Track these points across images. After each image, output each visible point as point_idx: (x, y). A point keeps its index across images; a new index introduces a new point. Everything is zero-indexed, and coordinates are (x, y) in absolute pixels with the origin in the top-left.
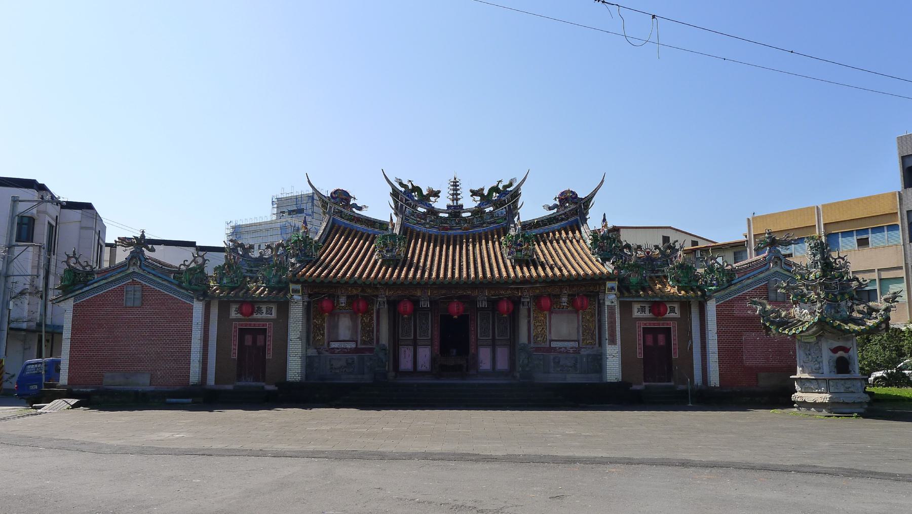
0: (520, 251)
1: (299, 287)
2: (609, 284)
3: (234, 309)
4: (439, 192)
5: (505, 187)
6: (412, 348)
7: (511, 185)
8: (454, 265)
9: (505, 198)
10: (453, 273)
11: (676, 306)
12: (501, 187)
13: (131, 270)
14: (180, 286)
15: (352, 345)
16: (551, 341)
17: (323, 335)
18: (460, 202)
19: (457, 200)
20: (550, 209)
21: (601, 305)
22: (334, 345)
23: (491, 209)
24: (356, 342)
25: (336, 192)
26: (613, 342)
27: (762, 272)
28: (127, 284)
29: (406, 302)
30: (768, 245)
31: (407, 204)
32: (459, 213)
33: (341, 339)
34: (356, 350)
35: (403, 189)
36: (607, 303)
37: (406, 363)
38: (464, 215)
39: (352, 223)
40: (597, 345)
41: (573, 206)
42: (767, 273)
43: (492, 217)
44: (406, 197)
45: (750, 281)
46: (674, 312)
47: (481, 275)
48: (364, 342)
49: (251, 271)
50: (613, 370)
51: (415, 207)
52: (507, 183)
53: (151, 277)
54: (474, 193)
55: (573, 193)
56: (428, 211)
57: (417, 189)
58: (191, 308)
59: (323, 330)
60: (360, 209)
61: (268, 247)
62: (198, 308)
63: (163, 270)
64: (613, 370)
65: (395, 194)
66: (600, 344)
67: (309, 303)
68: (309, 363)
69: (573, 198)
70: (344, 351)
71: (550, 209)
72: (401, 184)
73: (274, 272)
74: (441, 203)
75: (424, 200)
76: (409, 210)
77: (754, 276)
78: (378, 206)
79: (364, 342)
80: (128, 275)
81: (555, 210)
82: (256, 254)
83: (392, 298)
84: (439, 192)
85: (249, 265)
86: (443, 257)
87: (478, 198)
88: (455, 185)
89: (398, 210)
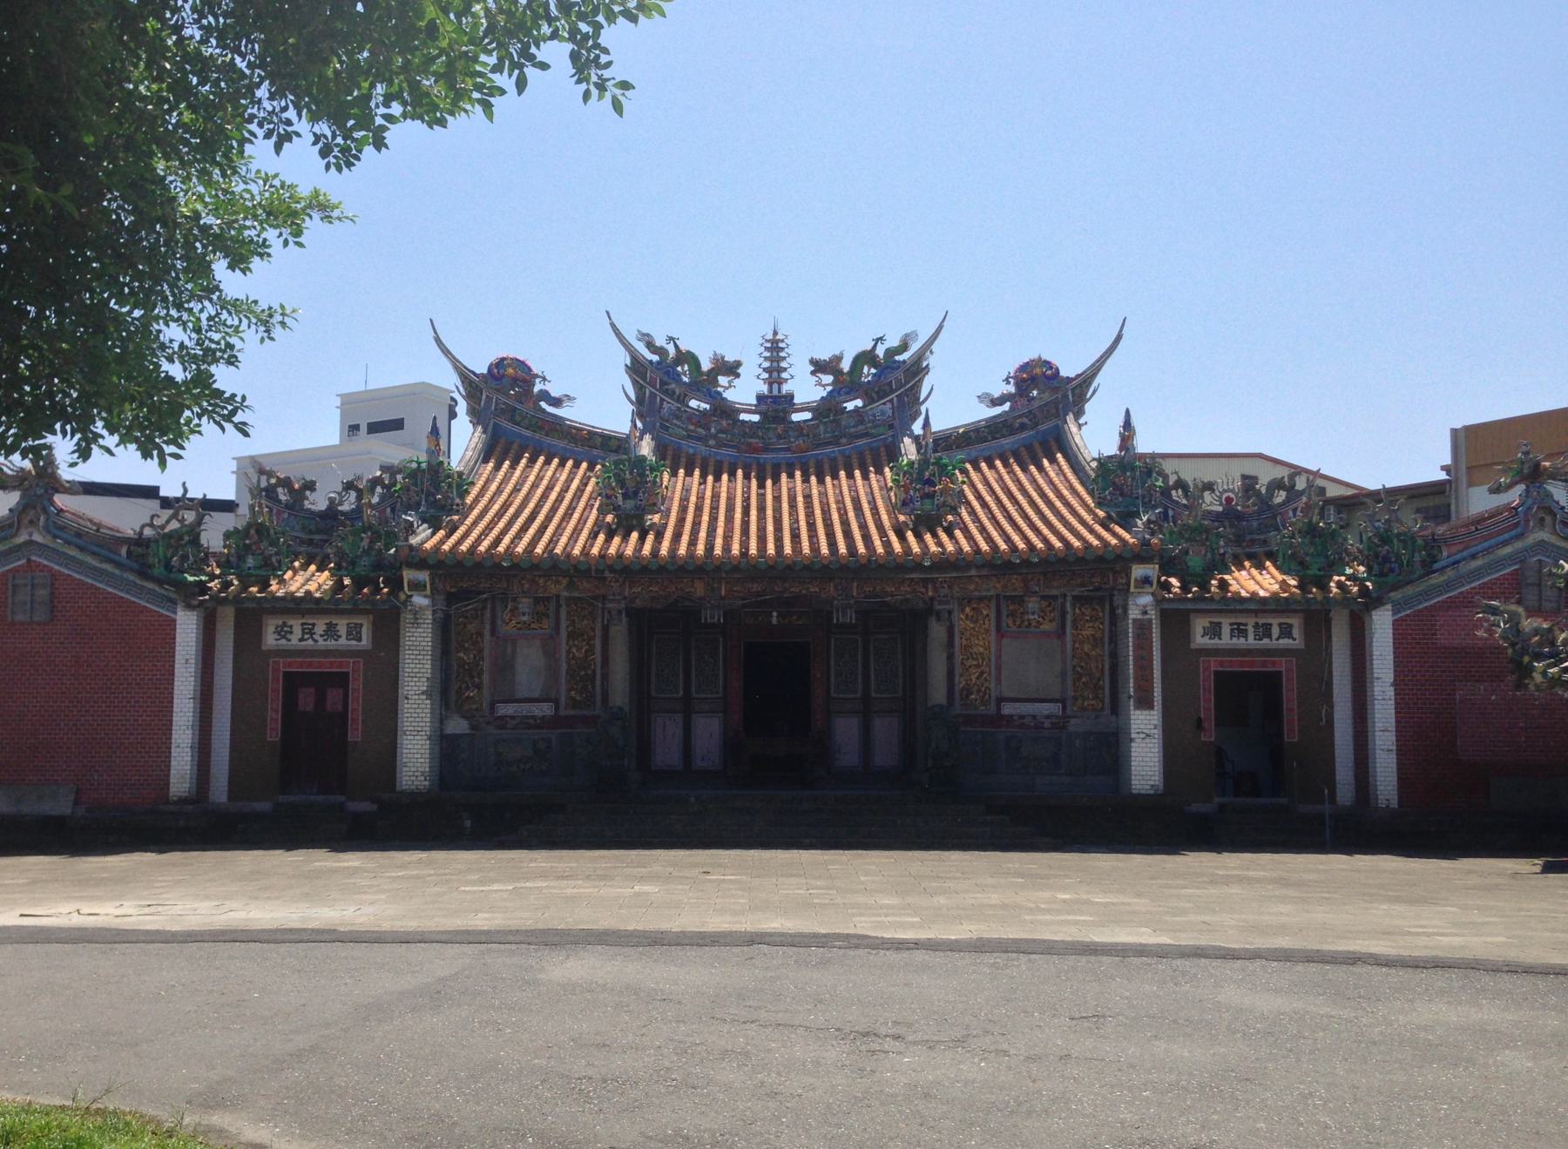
0: (931, 496)
1: (423, 576)
2: (1138, 571)
3: (271, 629)
4: (738, 364)
5: (891, 353)
6: (679, 717)
7: (904, 347)
9: (891, 379)
11: (1296, 622)
12: (880, 351)
14: (144, 573)
15: (546, 709)
16: (1001, 700)
17: (479, 687)
18: (786, 388)
19: (780, 382)
20: (995, 402)
21: (1116, 619)
23: (859, 403)
24: (556, 702)
25: (501, 363)
26: (1145, 703)
27: (1505, 543)
28: (16, 570)
29: (674, 614)
30: (1521, 478)
31: (666, 392)
33: (519, 695)
34: (555, 721)
35: (655, 358)
36: (1134, 613)
37: (667, 751)
38: (796, 417)
39: (537, 436)
40: (1107, 711)
41: (1047, 397)
42: (1519, 545)
43: (861, 422)
44: (663, 379)
45: (1479, 562)
46: (1289, 635)
47: (843, 549)
49: (310, 542)
50: (1145, 763)
51: (682, 400)
52: (555, 393)
53: (73, 552)
55: (1048, 364)
56: (714, 409)
57: (689, 358)
58: (171, 624)
59: (479, 676)
60: (557, 402)
61: (349, 486)
62: (187, 626)
64: (1145, 763)
65: (637, 368)
66: (1116, 708)
67: (447, 617)
68: (446, 748)
71: (995, 402)
72: (650, 345)
73: (365, 543)
74: (744, 391)
75: (705, 383)
76: (669, 405)
77: (1488, 550)
78: (601, 402)
81: (1007, 406)
82: (318, 502)
83: (639, 603)
84: (738, 364)
85: (303, 528)
87: (828, 379)
88: (775, 349)
89: (644, 407)
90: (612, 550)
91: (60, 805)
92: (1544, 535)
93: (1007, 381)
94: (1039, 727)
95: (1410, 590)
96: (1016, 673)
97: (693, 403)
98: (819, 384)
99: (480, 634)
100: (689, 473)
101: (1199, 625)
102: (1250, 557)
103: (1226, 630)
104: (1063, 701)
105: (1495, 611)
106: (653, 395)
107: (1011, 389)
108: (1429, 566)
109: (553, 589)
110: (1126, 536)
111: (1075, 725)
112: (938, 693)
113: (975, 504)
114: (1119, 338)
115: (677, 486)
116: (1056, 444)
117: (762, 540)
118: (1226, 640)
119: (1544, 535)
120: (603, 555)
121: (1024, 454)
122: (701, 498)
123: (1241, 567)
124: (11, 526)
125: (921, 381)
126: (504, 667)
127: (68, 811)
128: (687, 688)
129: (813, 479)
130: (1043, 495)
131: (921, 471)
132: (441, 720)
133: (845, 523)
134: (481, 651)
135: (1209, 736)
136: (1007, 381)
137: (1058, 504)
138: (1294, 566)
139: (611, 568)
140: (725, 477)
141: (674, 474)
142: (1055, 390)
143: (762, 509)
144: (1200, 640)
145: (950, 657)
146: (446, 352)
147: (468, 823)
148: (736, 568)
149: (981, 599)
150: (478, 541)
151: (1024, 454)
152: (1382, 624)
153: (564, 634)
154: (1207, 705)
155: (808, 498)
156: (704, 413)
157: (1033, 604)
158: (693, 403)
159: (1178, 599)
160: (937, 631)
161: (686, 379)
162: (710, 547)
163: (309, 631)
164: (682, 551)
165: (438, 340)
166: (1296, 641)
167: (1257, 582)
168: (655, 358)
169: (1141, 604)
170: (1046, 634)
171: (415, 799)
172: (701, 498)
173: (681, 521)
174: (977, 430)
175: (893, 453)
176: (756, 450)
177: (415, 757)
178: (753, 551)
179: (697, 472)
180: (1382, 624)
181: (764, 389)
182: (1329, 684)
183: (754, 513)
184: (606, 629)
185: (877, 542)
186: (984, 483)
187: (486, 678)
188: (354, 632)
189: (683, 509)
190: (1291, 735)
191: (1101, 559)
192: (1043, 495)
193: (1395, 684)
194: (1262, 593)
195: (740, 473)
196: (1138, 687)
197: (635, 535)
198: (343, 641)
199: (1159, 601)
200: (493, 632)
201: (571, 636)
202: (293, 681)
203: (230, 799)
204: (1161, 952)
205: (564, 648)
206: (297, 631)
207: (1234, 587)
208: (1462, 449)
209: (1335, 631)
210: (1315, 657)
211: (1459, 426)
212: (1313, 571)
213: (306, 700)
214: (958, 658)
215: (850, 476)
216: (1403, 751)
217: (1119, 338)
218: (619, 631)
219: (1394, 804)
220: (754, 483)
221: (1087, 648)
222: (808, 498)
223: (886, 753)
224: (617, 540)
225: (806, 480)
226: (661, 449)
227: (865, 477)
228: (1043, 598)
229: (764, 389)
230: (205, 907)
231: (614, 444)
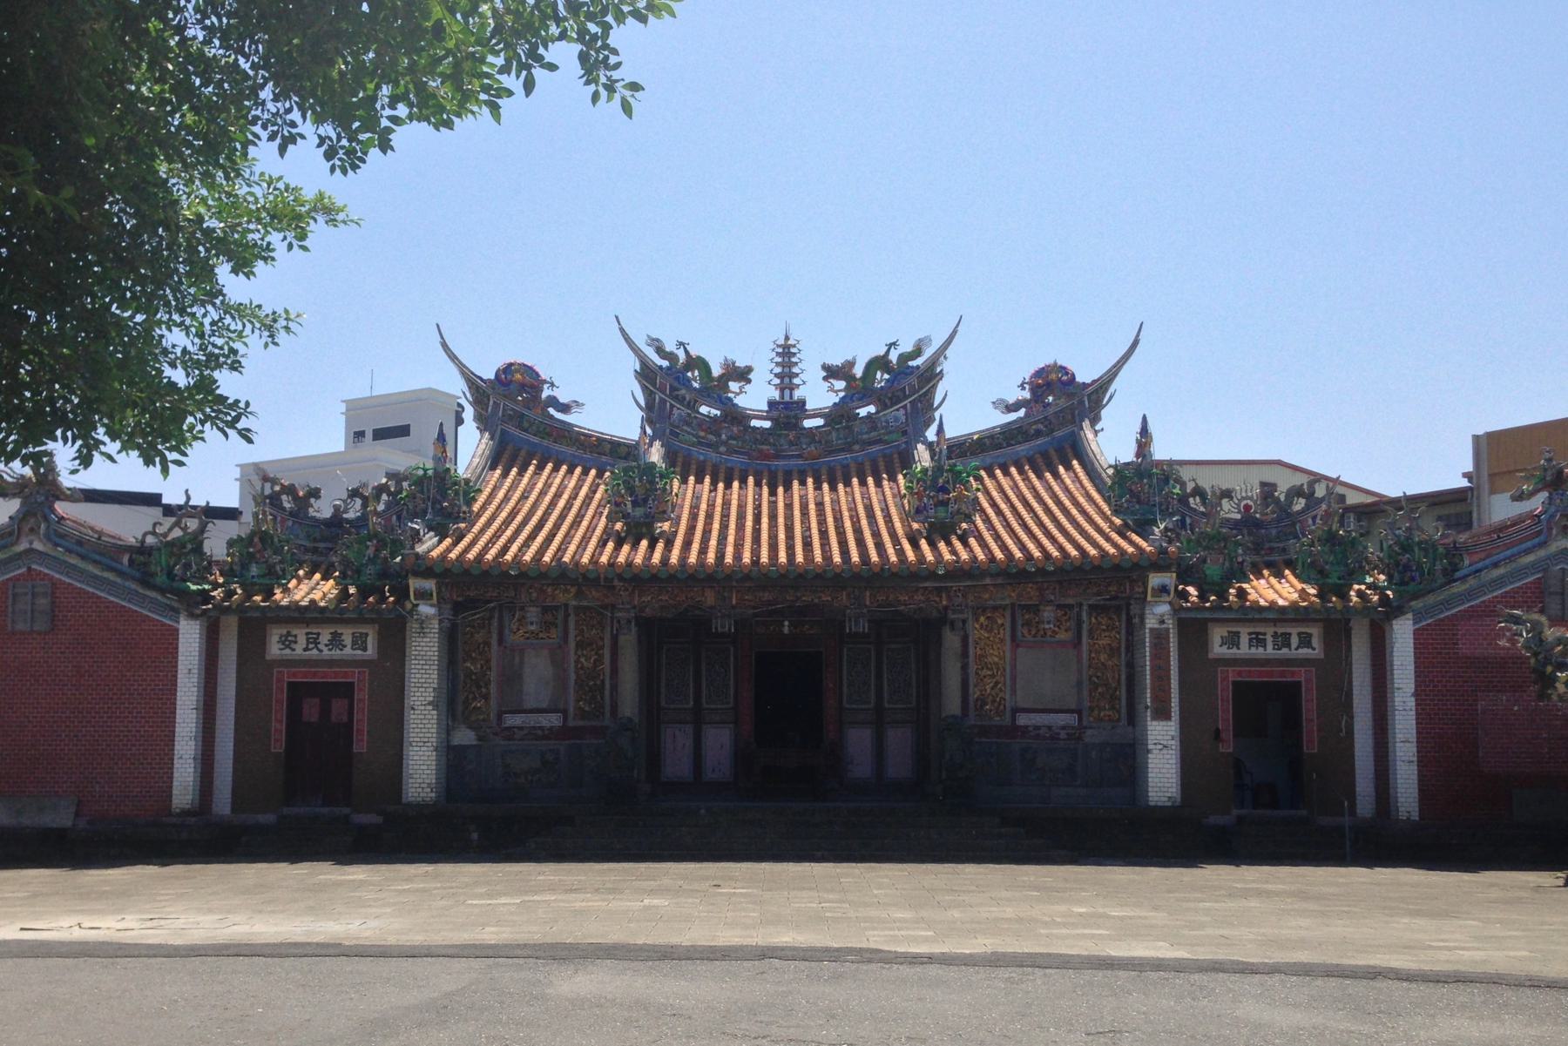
0: (945, 503)
1: (430, 585)
2: (1155, 580)
3: (275, 638)
4: (749, 369)
5: (904, 358)
6: (689, 729)
7: (917, 352)
8: (1041, 525)
9: (905, 385)
10: (756, 553)
11: (1315, 632)
12: (893, 357)
13: (23, 546)
14: (146, 581)
15: (554, 720)
16: (1016, 710)
17: (486, 697)
18: (797, 394)
19: (792, 388)
20: (1010, 408)
21: (1133, 627)
22: (513, 720)
23: (872, 409)
24: (565, 712)
25: (508, 368)
26: (1162, 713)
27: (1528, 551)
28: (17, 579)
31: (676, 398)
32: (799, 419)
34: (563, 733)
35: (665, 363)
36: (1151, 623)
37: (677, 763)
38: (808, 423)
39: (545, 443)
40: (1124, 721)
41: (1063, 403)
42: (1542, 553)
43: (874, 428)
44: (672, 385)
45: (1501, 571)
46: (1308, 644)
47: (855, 557)
48: (582, 714)
49: (315, 551)
50: (1163, 774)
51: (693, 406)
52: (563, 399)
53: (74, 560)
55: (1063, 369)
57: (700, 364)
58: (175, 633)
59: (487, 684)
60: (565, 408)
61: (354, 493)
62: (190, 636)
63: (103, 551)
64: (1163, 774)
65: (646, 374)
66: (1133, 718)
68: (453, 759)
69: (1064, 384)
70: (535, 733)
71: (1010, 408)
72: (660, 351)
73: (370, 552)
74: (755, 397)
75: (715, 389)
76: (679, 412)
77: (1512, 558)
78: (611, 409)
79: (582, 714)
80: (20, 555)
81: (1022, 413)
82: (322, 509)
84: (749, 369)
85: (308, 536)
86: (1050, 502)
87: (840, 385)
88: (786, 354)
89: (654, 413)
90: (621, 559)
91: (62, 818)
93: (1022, 387)
94: (1054, 738)
95: (1431, 599)
96: (1031, 683)
97: (704, 409)
98: (832, 389)
99: (487, 644)
100: (700, 481)
101: (1217, 634)
102: (1269, 565)
103: (1244, 640)
104: (1079, 712)
105: (1517, 620)
106: (663, 402)
107: (1027, 395)
108: (1450, 575)
109: (562, 598)
110: (1144, 544)
111: (1090, 736)
112: (952, 704)
113: (990, 511)
114: (1135, 343)
116: (1073, 450)
117: (773, 548)
118: (1245, 650)
120: (612, 564)
122: (711, 506)
123: (1259, 576)
124: (11, 534)
125: (934, 387)
126: (512, 678)
127: (69, 824)
129: (826, 486)
130: (1059, 503)
132: (447, 730)
133: (858, 531)
134: (488, 661)
135: (1227, 748)
136: (1022, 387)
137: (1074, 512)
138: (1313, 574)
139: (620, 577)
140: (736, 484)
141: (684, 481)
142: (1070, 396)
143: (773, 517)
144: (1218, 649)
145: (965, 667)
146: (453, 357)
147: (475, 836)
149: (995, 608)
150: (486, 549)
151: (1040, 460)
152: (1403, 633)
154: (1225, 716)
155: (820, 505)
156: (714, 419)
157: (1048, 613)
158: (704, 409)
160: (951, 640)
161: (696, 385)
162: (720, 555)
163: (314, 641)
164: (693, 559)
165: (444, 345)
166: (1316, 651)
167: (1276, 590)
168: (665, 363)
169: (1158, 613)
170: (1062, 644)
172: (711, 506)
174: (992, 437)
175: (907, 460)
176: (767, 457)
177: (421, 769)
179: (707, 480)
180: (1403, 633)
181: (776, 395)
183: (765, 520)
184: (615, 639)
185: (891, 551)
186: (999, 490)
187: (493, 688)
188: (359, 642)
189: (694, 517)
190: (1311, 745)
191: (1117, 567)
192: (1059, 503)
193: (1416, 694)
194: (1281, 602)
195: (751, 480)
196: (1155, 698)
197: (644, 543)
198: (348, 651)
199: (1176, 610)
200: (501, 641)
201: (579, 645)
202: (298, 692)
203: (233, 810)
205: (572, 658)
206: (302, 640)
207: (1253, 596)
208: (1484, 456)
211: (1481, 432)
212: (1333, 580)
214: (973, 668)
215: (863, 483)
217: (1135, 343)
219: (1415, 816)
220: (765, 490)
221: (1103, 657)
222: (820, 505)
223: (899, 765)
224: (626, 548)
225: (818, 487)
226: (670, 456)
227: (878, 484)
228: (1059, 607)
229: (776, 395)
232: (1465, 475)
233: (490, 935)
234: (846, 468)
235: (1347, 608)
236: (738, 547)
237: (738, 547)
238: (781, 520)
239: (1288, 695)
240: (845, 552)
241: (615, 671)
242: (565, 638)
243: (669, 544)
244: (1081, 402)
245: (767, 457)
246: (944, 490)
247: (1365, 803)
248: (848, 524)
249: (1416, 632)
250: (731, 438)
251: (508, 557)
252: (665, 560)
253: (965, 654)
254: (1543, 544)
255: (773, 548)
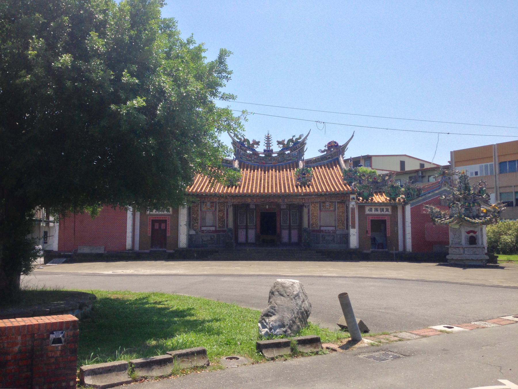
2: (352, 196)
4: (259, 142)
5: (297, 139)
6: (245, 230)
7: (300, 138)
8: (327, 182)
9: (297, 146)
11: (390, 208)
12: (294, 139)
15: (213, 229)
17: (197, 223)
18: (271, 148)
19: (270, 147)
20: (323, 152)
21: (347, 207)
23: (289, 152)
24: (216, 227)
26: (354, 227)
31: (241, 149)
34: (216, 231)
36: (351, 206)
37: (242, 238)
38: (273, 155)
41: (335, 150)
42: (440, 190)
43: (290, 157)
45: (430, 195)
50: (354, 241)
51: (245, 151)
54: (279, 143)
55: (335, 142)
56: (253, 154)
57: (248, 141)
59: (198, 220)
64: (354, 241)
66: (347, 228)
68: (190, 238)
70: (209, 232)
71: (323, 152)
74: (260, 149)
79: (220, 227)
81: (325, 153)
83: (235, 203)
84: (259, 142)
87: (281, 146)
88: (268, 138)
90: (229, 191)
91: (101, 251)
92: (445, 188)
93: (325, 146)
95: (414, 201)
96: (324, 219)
97: (248, 152)
98: (279, 147)
99: (198, 210)
100: (247, 170)
101: (367, 209)
102: (380, 192)
103: (373, 210)
104: (335, 227)
105: (427, 207)
106: (238, 150)
107: (327, 148)
108: (418, 196)
109: (215, 200)
110: (349, 188)
111: (338, 232)
112: (305, 225)
113: (316, 179)
114: (353, 136)
115: (245, 174)
116: (336, 162)
117: (264, 188)
118: (373, 212)
119: (445, 188)
120: (227, 192)
121: (329, 164)
122: (250, 176)
123: (377, 195)
125: (304, 147)
126: (203, 219)
127: (103, 252)
128: (247, 223)
129: (277, 171)
130: (332, 176)
131: (302, 172)
132: (188, 231)
133: (284, 184)
134: (198, 215)
135: (369, 235)
136: (325, 146)
137: (336, 179)
138: (388, 195)
139: (229, 196)
140: (256, 171)
141: (243, 170)
142: (337, 149)
143: (264, 180)
144: (367, 212)
145: (309, 216)
147: (196, 255)
148: (258, 196)
149: (316, 202)
150: (197, 189)
151: (329, 164)
152: (408, 208)
153: (217, 210)
154: (369, 228)
155: (276, 176)
156: (250, 154)
157: (327, 204)
158: (248, 152)
159: (361, 203)
160: (305, 210)
161: (246, 146)
162: (252, 190)
164: (245, 191)
166: (390, 212)
167: (379, 199)
168: (239, 141)
169: (352, 204)
170: (331, 211)
171: (183, 250)
172: (250, 176)
173: (245, 183)
174: (318, 159)
175: (297, 166)
176: (264, 164)
177: (183, 241)
178: (262, 192)
179: (249, 169)
180: (408, 208)
181: (266, 148)
182: (397, 222)
183: (262, 181)
184: (227, 210)
185: (291, 189)
186: (317, 173)
187: (199, 221)
189: (246, 179)
190: (388, 235)
191: (343, 194)
192: (332, 176)
193: (411, 223)
194: (381, 202)
195: (259, 169)
196: (352, 223)
197: (234, 187)
199: (357, 203)
200: (201, 210)
201: (219, 211)
202: (154, 222)
203: (139, 249)
204: (337, 277)
205: (217, 214)
207: (374, 200)
208: (453, 156)
209: (398, 210)
210: (394, 215)
211: (452, 151)
212: (393, 196)
213: (157, 226)
214: (311, 216)
215: (287, 170)
216: (413, 238)
217: (353, 136)
218: (231, 210)
219: (411, 251)
220: (263, 172)
221: (341, 214)
222: (276, 176)
223: (295, 239)
224: (230, 188)
225: (276, 172)
226: (240, 164)
227: (290, 171)
228: (331, 202)
229: (266, 148)
230: (143, 271)
231: (228, 162)
232: (449, 162)
233: (205, 273)
234: (283, 166)
235: (395, 204)
236: (256, 188)
237: (256, 188)
238: (266, 181)
239: (384, 222)
240: (281, 189)
241: (227, 217)
242: (216, 210)
243: (240, 187)
244: (340, 150)
245: (264, 164)
246: (304, 174)
247: (401, 249)
248: (282, 182)
249: (411, 209)
250: (255, 159)
251: (203, 191)
252: (239, 192)
253: (309, 213)
254: (440, 189)
255: (264, 188)
